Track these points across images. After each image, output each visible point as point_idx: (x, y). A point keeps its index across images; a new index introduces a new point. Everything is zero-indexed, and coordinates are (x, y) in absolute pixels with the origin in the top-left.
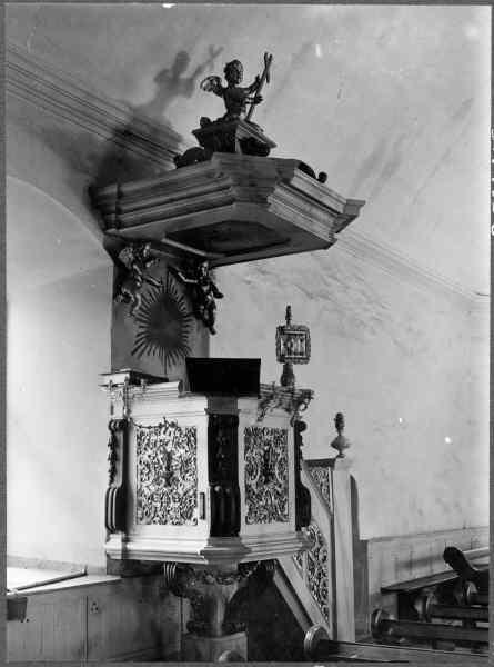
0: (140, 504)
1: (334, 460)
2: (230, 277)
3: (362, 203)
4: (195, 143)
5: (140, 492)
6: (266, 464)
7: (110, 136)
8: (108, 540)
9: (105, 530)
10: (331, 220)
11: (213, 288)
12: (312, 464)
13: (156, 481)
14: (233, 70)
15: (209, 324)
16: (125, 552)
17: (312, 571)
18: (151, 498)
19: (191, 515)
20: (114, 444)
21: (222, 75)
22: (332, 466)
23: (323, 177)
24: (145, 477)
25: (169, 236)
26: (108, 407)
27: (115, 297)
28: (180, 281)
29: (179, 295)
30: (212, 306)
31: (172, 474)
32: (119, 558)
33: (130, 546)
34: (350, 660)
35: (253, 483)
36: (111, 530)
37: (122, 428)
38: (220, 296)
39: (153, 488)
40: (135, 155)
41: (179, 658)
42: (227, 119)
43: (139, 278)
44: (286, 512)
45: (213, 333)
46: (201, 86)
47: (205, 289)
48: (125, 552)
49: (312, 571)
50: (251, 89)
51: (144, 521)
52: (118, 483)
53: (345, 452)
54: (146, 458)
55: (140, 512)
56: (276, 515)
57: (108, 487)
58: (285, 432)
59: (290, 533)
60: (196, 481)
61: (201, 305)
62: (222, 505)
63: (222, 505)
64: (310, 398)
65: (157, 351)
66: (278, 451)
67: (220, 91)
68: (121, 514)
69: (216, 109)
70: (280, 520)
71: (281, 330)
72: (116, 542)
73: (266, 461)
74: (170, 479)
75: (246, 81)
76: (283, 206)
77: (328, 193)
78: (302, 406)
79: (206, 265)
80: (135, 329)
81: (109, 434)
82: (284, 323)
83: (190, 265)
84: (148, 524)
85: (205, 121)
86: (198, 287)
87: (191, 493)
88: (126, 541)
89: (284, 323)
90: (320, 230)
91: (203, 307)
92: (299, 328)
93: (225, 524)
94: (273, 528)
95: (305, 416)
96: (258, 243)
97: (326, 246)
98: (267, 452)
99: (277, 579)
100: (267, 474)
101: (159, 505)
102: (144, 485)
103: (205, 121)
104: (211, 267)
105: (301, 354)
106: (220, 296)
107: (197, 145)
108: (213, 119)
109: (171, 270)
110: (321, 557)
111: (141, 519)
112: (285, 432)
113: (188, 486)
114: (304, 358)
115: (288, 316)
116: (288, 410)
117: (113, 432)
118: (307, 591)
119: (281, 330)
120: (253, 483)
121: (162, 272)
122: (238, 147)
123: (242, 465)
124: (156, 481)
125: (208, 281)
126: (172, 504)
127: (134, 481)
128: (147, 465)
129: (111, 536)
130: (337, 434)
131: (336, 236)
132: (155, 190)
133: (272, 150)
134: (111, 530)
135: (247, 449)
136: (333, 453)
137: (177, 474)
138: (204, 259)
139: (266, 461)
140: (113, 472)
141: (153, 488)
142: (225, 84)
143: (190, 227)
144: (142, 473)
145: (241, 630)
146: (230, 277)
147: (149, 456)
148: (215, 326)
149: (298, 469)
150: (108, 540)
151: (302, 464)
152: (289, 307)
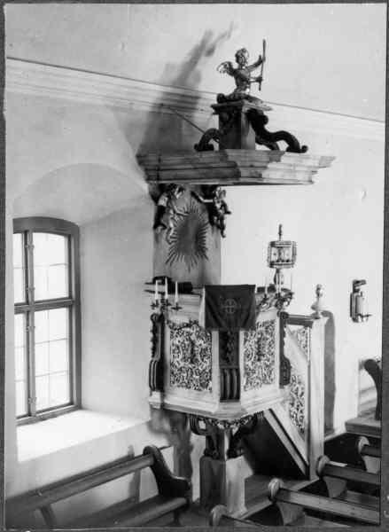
3: (333, 159)
4: (214, 122)
5: (172, 364)
6: (259, 348)
8: (151, 395)
11: (224, 205)
13: (184, 359)
14: (240, 56)
15: (222, 228)
16: (163, 405)
17: (293, 404)
18: (180, 369)
19: (207, 385)
20: (154, 331)
24: (176, 355)
28: (199, 200)
29: (200, 211)
30: (222, 219)
31: (195, 355)
32: (159, 407)
33: (166, 401)
34: (289, 503)
36: (153, 389)
37: (159, 322)
39: (182, 364)
41: (223, 367)
42: (235, 337)
43: (171, 212)
46: (217, 69)
47: (218, 206)
48: (163, 405)
49: (293, 404)
50: (256, 65)
51: (176, 384)
52: (157, 358)
55: (172, 379)
56: (265, 380)
57: (151, 359)
58: (272, 322)
59: (276, 391)
60: (211, 363)
62: (228, 377)
63: (228, 377)
66: (268, 336)
67: (232, 72)
68: (159, 377)
70: (268, 383)
72: (157, 395)
73: (259, 345)
74: (193, 360)
75: (252, 60)
78: (286, 303)
80: (166, 247)
81: (150, 324)
83: (209, 192)
84: (179, 386)
85: (221, 98)
87: (207, 371)
88: (163, 397)
89: (275, 238)
91: (216, 218)
93: (230, 393)
98: (259, 340)
101: (185, 375)
102: (175, 359)
105: (288, 261)
106: (229, 213)
107: (218, 128)
110: (300, 393)
111: (174, 383)
112: (272, 322)
113: (205, 365)
114: (289, 263)
115: (280, 234)
117: (154, 323)
118: (288, 418)
120: (249, 363)
123: (242, 351)
124: (184, 359)
126: (194, 376)
127: (169, 357)
130: (316, 300)
135: (246, 340)
139: (259, 345)
140: (154, 349)
142: (235, 66)
145: (240, 455)
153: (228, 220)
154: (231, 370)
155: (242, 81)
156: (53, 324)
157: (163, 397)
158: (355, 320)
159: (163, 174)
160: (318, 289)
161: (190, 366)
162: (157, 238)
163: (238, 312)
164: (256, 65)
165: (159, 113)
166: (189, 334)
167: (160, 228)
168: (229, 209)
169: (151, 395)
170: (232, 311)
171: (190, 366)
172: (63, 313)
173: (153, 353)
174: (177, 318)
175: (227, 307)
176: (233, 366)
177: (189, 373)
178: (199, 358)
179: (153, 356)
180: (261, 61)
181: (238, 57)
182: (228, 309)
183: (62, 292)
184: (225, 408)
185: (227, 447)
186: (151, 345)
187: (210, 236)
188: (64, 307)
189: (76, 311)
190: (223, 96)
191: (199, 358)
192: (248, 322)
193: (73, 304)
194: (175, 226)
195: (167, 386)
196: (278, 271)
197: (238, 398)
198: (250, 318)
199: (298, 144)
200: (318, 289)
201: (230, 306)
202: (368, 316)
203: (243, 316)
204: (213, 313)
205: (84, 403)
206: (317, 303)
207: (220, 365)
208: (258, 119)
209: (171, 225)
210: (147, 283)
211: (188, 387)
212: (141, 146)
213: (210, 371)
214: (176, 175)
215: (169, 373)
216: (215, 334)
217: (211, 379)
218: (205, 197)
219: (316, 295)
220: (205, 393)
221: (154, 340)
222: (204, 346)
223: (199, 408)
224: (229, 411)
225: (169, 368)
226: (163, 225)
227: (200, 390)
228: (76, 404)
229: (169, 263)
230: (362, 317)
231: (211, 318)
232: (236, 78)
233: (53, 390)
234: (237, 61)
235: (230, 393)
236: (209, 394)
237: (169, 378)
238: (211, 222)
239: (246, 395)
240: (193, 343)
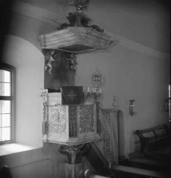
8: (43, 136)
9: (42, 133)
12: (103, 111)
16: (47, 140)
23: (103, 31)
26: (42, 101)
33: (49, 139)
36: (44, 134)
40: (73, 42)
41: (70, 122)
48: (47, 140)
57: (43, 121)
65: (58, 81)
66: (91, 111)
68: (46, 128)
72: (45, 136)
77: (104, 35)
78: (98, 98)
84: (53, 132)
85: (70, 14)
86: (70, 61)
88: (48, 136)
101: (56, 127)
102: (52, 121)
108: (72, 13)
129: (44, 135)
132: (70, 41)
133: (90, 22)
134: (44, 134)
140: (44, 117)
143: (64, 46)
144: (52, 118)
147: (54, 113)
149: (98, 111)
151: (100, 111)
157: (48, 136)
158: (132, 115)
161: (58, 123)
166: (57, 110)
169: (43, 136)
173: (44, 119)
174: (52, 103)
175: (70, 95)
177: (58, 126)
179: (44, 120)
182: (71, 96)
184: (71, 140)
186: (43, 115)
189: (14, 103)
190: (71, 13)
195: (50, 133)
199: (100, 29)
202: (136, 113)
207: (69, 122)
213: (65, 125)
214: (53, 44)
215: (50, 127)
218: (68, 58)
221: (44, 113)
222: (63, 114)
223: (60, 141)
227: (61, 133)
228: (12, 141)
229: (52, 82)
230: (134, 113)
237: (50, 129)
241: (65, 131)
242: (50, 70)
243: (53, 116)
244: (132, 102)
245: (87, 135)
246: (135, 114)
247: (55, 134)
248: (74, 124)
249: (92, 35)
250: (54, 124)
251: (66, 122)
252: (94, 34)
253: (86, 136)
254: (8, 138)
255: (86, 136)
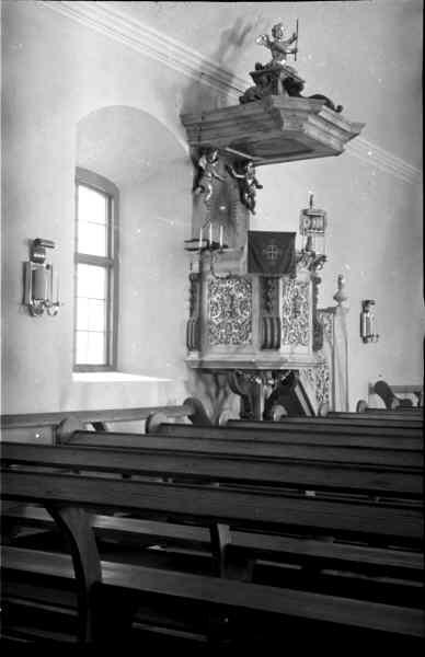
0: (210, 330)
1: (335, 308)
2: (264, 173)
4: (251, 83)
5: (210, 323)
7: (190, 75)
10: (341, 137)
11: (255, 182)
13: (223, 315)
15: (250, 206)
21: (270, 33)
22: (334, 313)
23: (339, 109)
25: (231, 147)
27: (194, 189)
28: (232, 176)
29: (232, 187)
30: (252, 196)
35: (288, 317)
36: (190, 348)
37: (197, 280)
38: (259, 187)
43: (210, 175)
44: (90, 428)
45: (254, 213)
47: (250, 182)
48: (201, 363)
49: (319, 386)
50: (291, 42)
52: (195, 318)
53: (343, 303)
54: (215, 299)
61: (245, 195)
62: (276, 334)
64: (324, 261)
68: (197, 335)
69: (266, 57)
71: (305, 212)
72: (194, 356)
74: (232, 314)
75: (287, 36)
76: (313, 130)
79: (250, 164)
81: (189, 284)
82: (308, 207)
85: (258, 66)
86: (244, 181)
88: (201, 356)
89: (308, 207)
90: (334, 143)
92: (319, 211)
94: (300, 349)
95: (320, 273)
96: (288, 150)
97: (338, 154)
99: (297, 389)
100: (296, 311)
102: (213, 317)
103: (258, 66)
104: (254, 166)
105: (319, 229)
106: (259, 187)
107: (254, 85)
108: (264, 64)
109: (227, 168)
116: (310, 269)
119: (305, 212)
121: (222, 171)
122: (280, 87)
125: (252, 176)
127: (207, 315)
128: (217, 304)
131: (345, 146)
134: (190, 348)
136: (334, 303)
137: (238, 311)
138: (248, 161)
140: (192, 310)
141: (220, 321)
146: (264, 173)
148: (255, 210)
150: (188, 354)
152: (312, 197)
153: (259, 196)
154: (272, 320)
155: (277, 50)
156: (93, 281)
159: (205, 134)
160: (340, 279)
162: (196, 200)
163: (280, 259)
164: (291, 42)
165: (198, 82)
166: (229, 289)
167: (199, 189)
168: (260, 183)
170: (272, 258)
171: (229, 321)
172: (101, 272)
176: (273, 315)
178: (239, 312)
180: (295, 38)
181: (274, 31)
183: (102, 252)
185: (262, 409)
187: (239, 209)
188: (101, 265)
191: (239, 312)
192: (290, 270)
193: (111, 264)
194: (214, 190)
195: (203, 347)
196: (309, 239)
197: (278, 347)
198: (291, 264)
200: (340, 279)
201: (272, 253)
203: (285, 262)
204: (255, 256)
205: (119, 366)
206: (338, 293)
208: (293, 87)
209: (210, 187)
210: (187, 242)
211: (227, 343)
212: (187, 92)
213: (250, 323)
216: (256, 283)
217: (251, 330)
218: (238, 173)
219: (336, 285)
220: (245, 346)
221: (192, 301)
224: (265, 359)
225: (208, 327)
226: (203, 188)
228: (110, 365)
231: (253, 262)
232: (272, 50)
233: (92, 349)
234: (274, 36)
235: (271, 344)
236: (249, 346)
237: (206, 336)
238: (243, 201)
239: (285, 348)
240: (232, 298)
241: (250, 337)
242: (209, 196)
243: (217, 304)
244: (366, 304)
245: (295, 351)
246: (375, 338)
247: (222, 347)
248: (275, 322)
249: (320, 117)
250: (217, 323)
251: (251, 317)
252: (324, 116)
253: (293, 353)
254: (100, 360)
255: (293, 353)
